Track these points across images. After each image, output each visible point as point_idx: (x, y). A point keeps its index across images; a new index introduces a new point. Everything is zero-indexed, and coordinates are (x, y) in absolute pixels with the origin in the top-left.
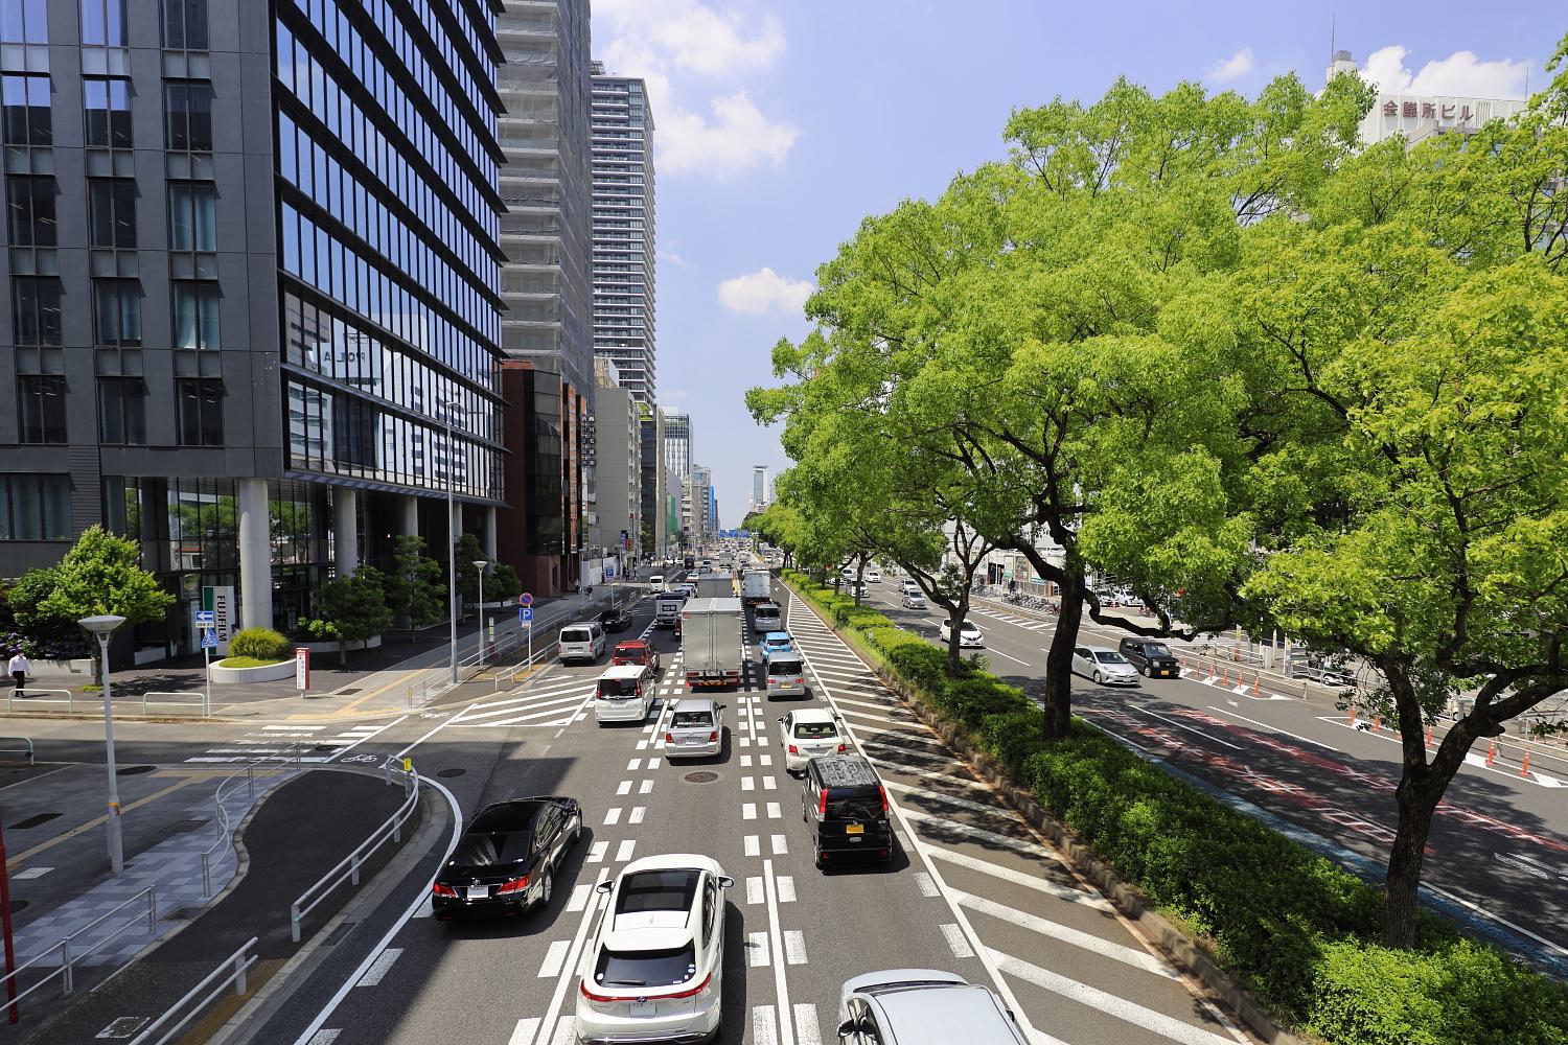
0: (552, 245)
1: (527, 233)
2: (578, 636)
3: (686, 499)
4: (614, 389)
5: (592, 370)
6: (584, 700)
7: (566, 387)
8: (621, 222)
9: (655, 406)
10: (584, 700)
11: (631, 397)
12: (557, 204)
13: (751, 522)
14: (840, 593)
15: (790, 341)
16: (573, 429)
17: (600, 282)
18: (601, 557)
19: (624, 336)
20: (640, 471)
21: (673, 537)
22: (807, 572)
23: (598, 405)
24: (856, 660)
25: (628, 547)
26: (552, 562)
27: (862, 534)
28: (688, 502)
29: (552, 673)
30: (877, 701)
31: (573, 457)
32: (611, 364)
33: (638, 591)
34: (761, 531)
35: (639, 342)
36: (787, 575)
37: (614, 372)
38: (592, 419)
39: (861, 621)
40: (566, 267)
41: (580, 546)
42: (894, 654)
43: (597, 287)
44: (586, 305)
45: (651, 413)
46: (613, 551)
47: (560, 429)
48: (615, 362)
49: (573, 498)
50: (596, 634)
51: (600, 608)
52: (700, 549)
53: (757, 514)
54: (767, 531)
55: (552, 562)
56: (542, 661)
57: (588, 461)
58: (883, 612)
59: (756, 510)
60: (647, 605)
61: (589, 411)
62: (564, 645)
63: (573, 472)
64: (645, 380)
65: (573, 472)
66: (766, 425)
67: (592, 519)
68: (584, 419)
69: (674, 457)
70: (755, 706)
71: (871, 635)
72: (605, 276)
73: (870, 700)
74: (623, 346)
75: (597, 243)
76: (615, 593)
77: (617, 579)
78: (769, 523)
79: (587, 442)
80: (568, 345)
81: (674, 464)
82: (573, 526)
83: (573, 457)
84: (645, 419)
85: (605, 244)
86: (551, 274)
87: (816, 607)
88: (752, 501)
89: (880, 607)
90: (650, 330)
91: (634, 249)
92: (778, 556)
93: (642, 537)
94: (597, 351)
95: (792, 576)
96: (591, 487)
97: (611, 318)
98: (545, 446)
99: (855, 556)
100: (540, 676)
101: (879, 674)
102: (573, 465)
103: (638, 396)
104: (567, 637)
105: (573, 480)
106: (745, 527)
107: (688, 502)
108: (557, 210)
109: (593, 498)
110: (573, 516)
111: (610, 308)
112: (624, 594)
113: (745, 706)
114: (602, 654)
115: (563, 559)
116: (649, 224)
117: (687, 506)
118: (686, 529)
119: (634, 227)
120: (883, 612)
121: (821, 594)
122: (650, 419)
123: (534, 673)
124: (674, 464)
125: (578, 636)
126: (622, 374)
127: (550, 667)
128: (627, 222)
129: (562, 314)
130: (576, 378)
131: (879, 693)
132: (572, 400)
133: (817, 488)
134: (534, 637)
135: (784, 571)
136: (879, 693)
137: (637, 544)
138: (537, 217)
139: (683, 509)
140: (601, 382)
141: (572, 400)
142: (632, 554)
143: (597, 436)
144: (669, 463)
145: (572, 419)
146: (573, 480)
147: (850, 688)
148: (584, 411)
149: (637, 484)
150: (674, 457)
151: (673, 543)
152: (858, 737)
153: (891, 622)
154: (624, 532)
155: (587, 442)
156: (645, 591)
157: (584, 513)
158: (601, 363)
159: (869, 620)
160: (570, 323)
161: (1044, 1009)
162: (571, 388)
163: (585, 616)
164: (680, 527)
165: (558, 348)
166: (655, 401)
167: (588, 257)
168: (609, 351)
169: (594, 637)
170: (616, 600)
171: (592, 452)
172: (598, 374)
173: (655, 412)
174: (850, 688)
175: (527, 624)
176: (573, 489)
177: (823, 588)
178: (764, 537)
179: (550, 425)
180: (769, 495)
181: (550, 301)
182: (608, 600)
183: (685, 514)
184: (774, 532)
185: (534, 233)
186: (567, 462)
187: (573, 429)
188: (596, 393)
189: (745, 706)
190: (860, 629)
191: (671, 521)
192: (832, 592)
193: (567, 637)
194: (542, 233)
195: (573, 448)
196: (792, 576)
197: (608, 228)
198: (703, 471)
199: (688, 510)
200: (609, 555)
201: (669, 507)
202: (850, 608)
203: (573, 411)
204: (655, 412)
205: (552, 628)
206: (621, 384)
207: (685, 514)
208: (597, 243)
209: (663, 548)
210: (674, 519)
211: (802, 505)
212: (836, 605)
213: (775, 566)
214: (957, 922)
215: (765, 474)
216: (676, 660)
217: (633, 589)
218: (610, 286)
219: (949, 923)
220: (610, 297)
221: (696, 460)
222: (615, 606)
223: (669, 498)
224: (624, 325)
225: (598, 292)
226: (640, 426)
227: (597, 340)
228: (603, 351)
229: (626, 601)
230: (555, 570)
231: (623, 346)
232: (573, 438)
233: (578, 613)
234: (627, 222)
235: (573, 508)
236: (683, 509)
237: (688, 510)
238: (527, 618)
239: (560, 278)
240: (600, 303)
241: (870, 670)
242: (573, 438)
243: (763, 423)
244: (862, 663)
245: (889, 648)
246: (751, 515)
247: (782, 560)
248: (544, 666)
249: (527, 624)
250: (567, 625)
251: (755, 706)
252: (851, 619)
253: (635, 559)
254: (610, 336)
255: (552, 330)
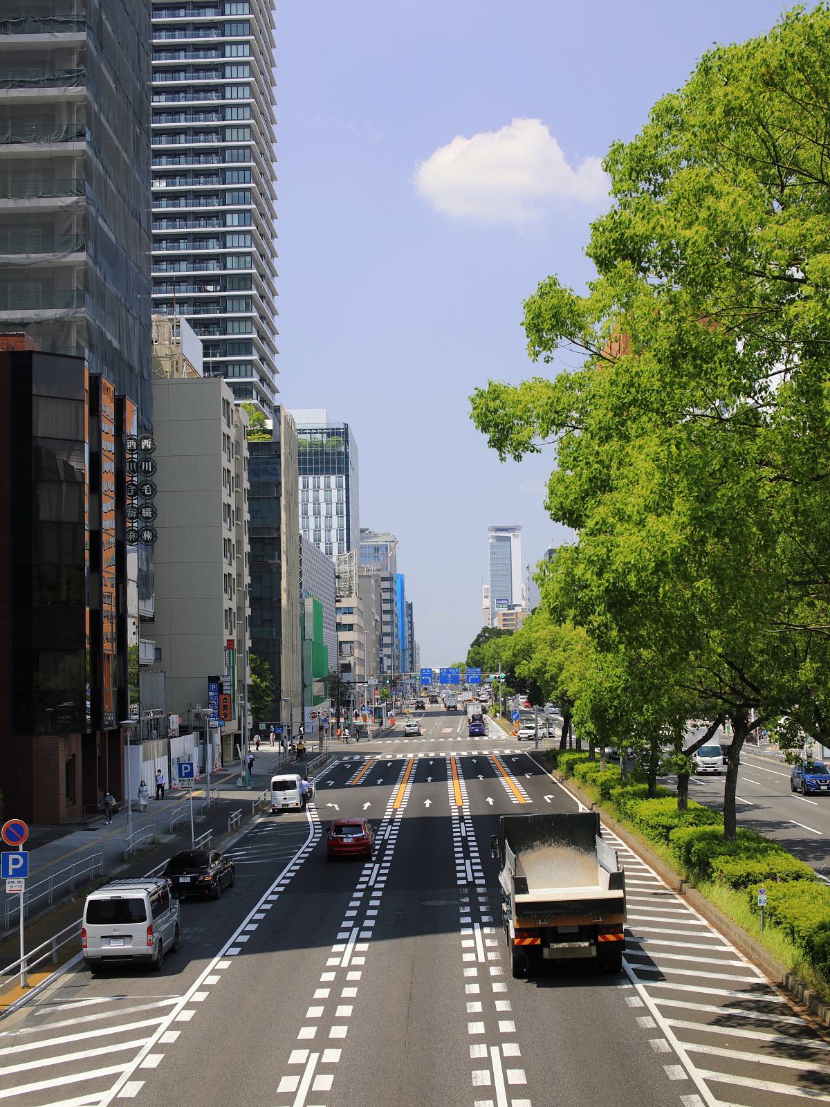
0: (70, 104)
1: (22, 84)
2: (122, 911)
3: (345, 603)
4: (192, 380)
5: (147, 342)
6: (136, 1051)
7: (95, 381)
8: (207, 47)
9: (277, 410)
10: (136, 1051)
11: (227, 394)
12: (81, 25)
13: (488, 649)
14: (691, 804)
15: (564, 283)
16: (108, 466)
17: (164, 166)
18: (165, 735)
19: (213, 270)
20: (247, 548)
21: (318, 688)
22: (613, 758)
23: (161, 412)
24: (732, 956)
25: (224, 714)
26: (66, 749)
27: (727, 674)
28: (349, 611)
29: (70, 991)
30: (777, 1048)
31: (109, 523)
32: (186, 328)
33: (247, 808)
34: (510, 669)
35: (245, 281)
36: (570, 767)
37: (192, 346)
38: (146, 444)
39: (741, 867)
40: (96, 145)
41: (122, 713)
42: (817, 940)
43: (160, 175)
44: (136, 215)
45: (269, 424)
46: (194, 723)
47: (83, 465)
48: (194, 324)
49: (109, 608)
50: (160, 905)
51: (167, 846)
52: (377, 713)
53: (497, 633)
54: (522, 670)
55: (66, 749)
56: (47, 966)
57: (139, 533)
58: (790, 846)
59: (498, 623)
60: (264, 839)
61: (141, 427)
62: (94, 931)
63: (108, 555)
64: (255, 357)
65: (108, 555)
66: (518, 458)
67: (147, 654)
68: (131, 444)
69: (317, 514)
70: (508, 1063)
71: (763, 899)
72: (173, 154)
73: (762, 1047)
74: (211, 291)
75: (158, 91)
76: (198, 812)
77: (201, 783)
78: (527, 652)
79: (138, 491)
80: (101, 297)
81: (317, 529)
82: (109, 670)
83: (109, 523)
84: (255, 439)
85: (173, 91)
86: (67, 159)
87: (639, 837)
88: (487, 603)
89: (780, 834)
90: (266, 256)
91: (232, 76)
92: (549, 723)
93: (253, 689)
94: (158, 303)
95: (581, 768)
96: (145, 582)
97: (184, 236)
98: (48, 505)
99: (720, 721)
100: (43, 997)
101: (783, 987)
102: (109, 539)
103: (242, 391)
104: (102, 912)
105: (109, 572)
106: (476, 661)
107: (349, 611)
108: (82, 36)
109: (149, 608)
110: (109, 647)
111: (184, 217)
112: (217, 815)
113: (486, 1064)
114: (172, 950)
115: (88, 742)
116: (262, 68)
117: (346, 619)
118: (347, 668)
119: (231, 55)
120: (790, 846)
121: (648, 808)
122: (267, 438)
123: (30, 993)
124: (317, 529)
125: (122, 911)
126: (208, 347)
127: (63, 978)
128: (219, 48)
129: (88, 237)
130: (113, 359)
131: (783, 1030)
132: (108, 407)
133: (618, 600)
134: (31, 912)
135: (564, 758)
136: (783, 1030)
137: (242, 704)
138: (44, 52)
139: (340, 626)
140: (166, 366)
141: (108, 407)
142: (232, 727)
143: (157, 479)
144: (308, 526)
145: (108, 445)
146: (109, 572)
147: (720, 1021)
148: (132, 428)
149: (240, 575)
150: (317, 514)
151: (317, 700)
152: (698, 1065)
153: (807, 867)
154: (214, 679)
155: (138, 491)
156: (261, 807)
157: (132, 640)
158: (167, 329)
159: (758, 866)
160: (104, 252)
161: (720, 1091)
162: (107, 384)
163: (133, 867)
164: (332, 664)
165: (82, 303)
166: (277, 400)
167: (141, 120)
168: (182, 302)
169: (156, 914)
170: (200, 829)
171: (147, 513)
172: (160, 350)
173: (277, 421)
174: (720, 1021)
175: (16, 886)
176: (109, 589)
177: (651, 794)
178: (516, 684)
179: (62, 457)
180: (522, 593)
181: (65, 211)
182: (182, 828)
183: (344, 636)
184: (540, 672)
185: (36, 84)
186: (96, 536)
187: (108, 466)
188: (158, 391)
189: (486, 1064)
190: (739, 884)
191: (312, 651)
192: (671, 804)
193: (102, 912)
194: (51, 83)
195: (108, 505)
196: (581, 768)
197: (182, 60)
198: (380, 541)
199: (350, 627)
200: (184, 730)
201: (309, 624)
202: (713, 836)
203: (108, 427)
204: (277, 421)
205: (65, 891)
206: (206, 366)
207: (344, 636)
208: (158, 91)
209: (297, 712)
210: (319, 646)
211: (595, 620)
212: (683, 833)
213: (545, 746)
214: (639, 995)
215: (516, 543)
216: (332, 962)
217: (235, 804)
218: (183, 174)
219: (674, 1064)
220: (185, 194)
221: (365, 517)
222: (199, 842)
223: (309, 603)
224: (213, 248)
225: (160, 186)
226: (246, 454)
227: (158, 282)
228: (170, 303)
229: (220, 831)
230: (70, 765)
231: (211, 291)
232: (108, 484)
233: (120, 858)
234: (219, 48)
235: (108, 628)
236: (340, 626)
237: (350, 627)
238: (17, 873)
239: (86, 165)
240: (164, 208)
241: (763, 980)
242: (108, 484)
243: (509, 457)
244: (744, 963)
245: (804, 926)
246: (488, 634)
247: (558, 732)
248: (50, 976)
249: (16, 886)
250: (98, 887)
251: (508, 1063)
252: (716, 863)
253: (237, 738)
254: (183, 271)
255: (69, 268)
